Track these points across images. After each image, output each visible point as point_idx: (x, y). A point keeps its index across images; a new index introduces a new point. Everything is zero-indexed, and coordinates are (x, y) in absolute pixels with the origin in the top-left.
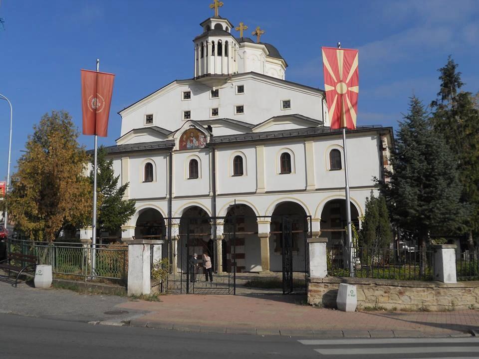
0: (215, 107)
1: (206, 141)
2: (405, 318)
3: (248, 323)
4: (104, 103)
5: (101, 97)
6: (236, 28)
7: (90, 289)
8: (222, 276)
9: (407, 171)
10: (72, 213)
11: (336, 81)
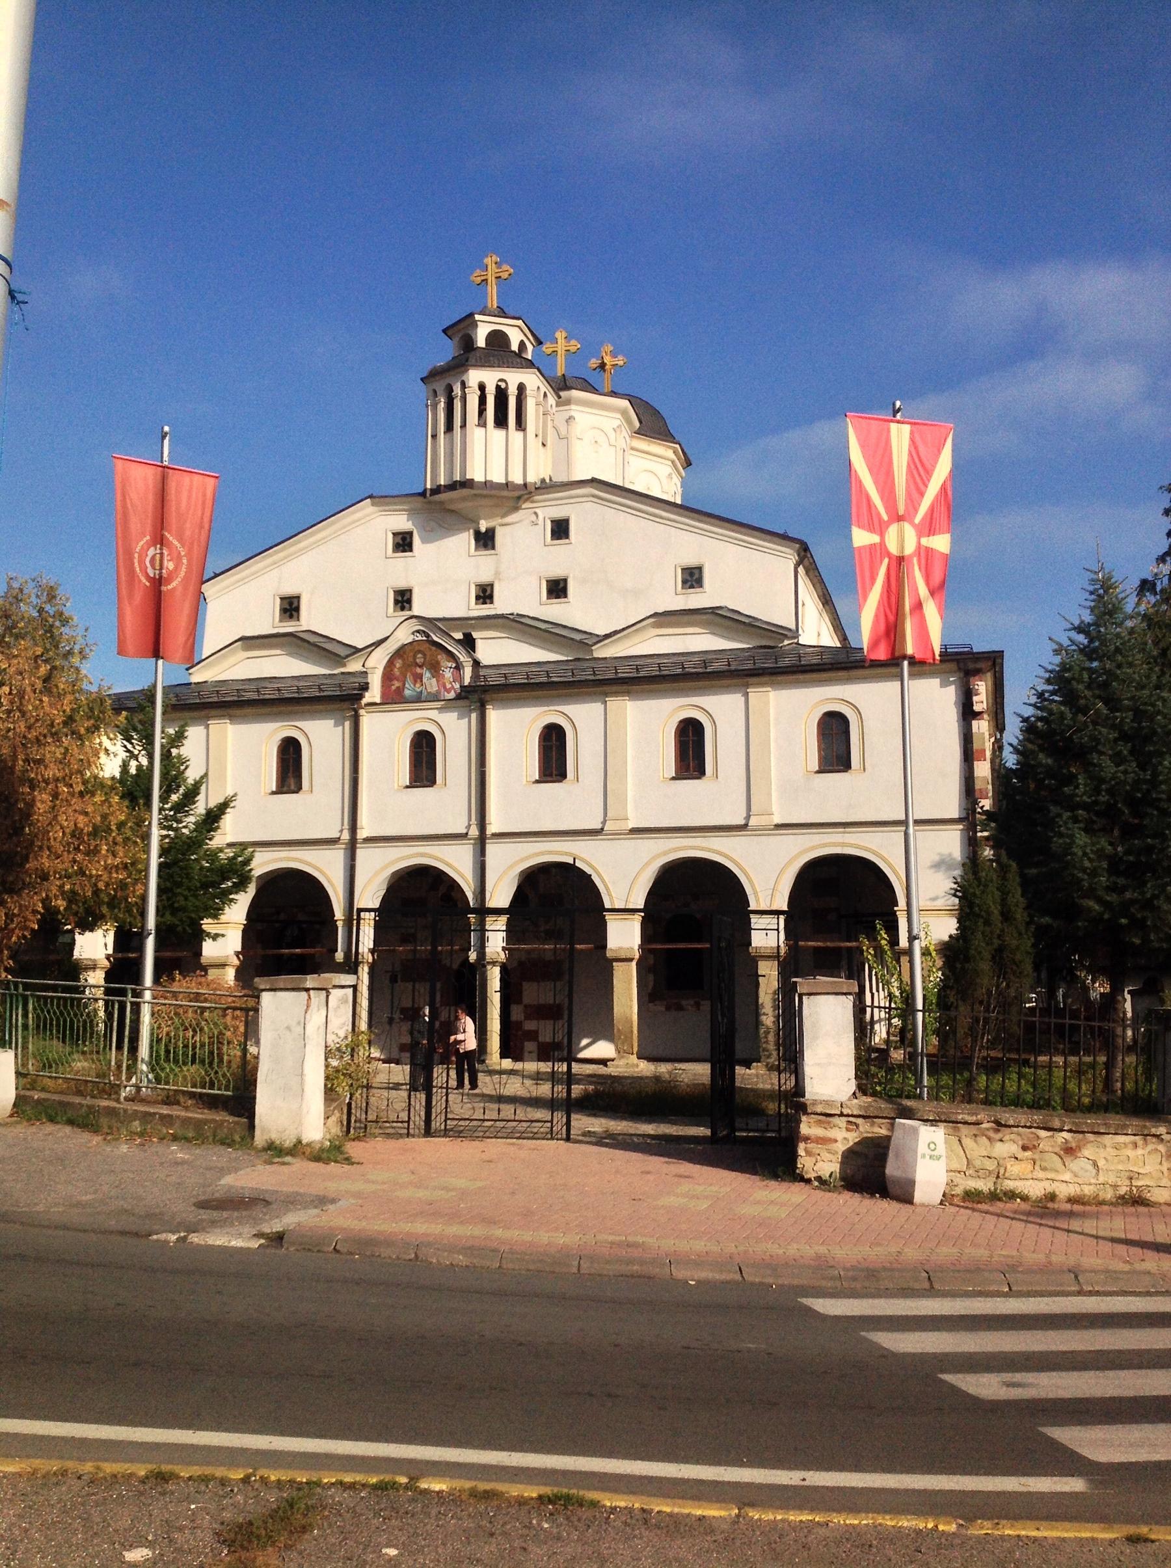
0: (485, 578)
1: (461, 679)
2: (1089, 1226)
3: (640, 1239)
4: (185, 561)
5: (176, 542)
6: (547, 348)
7: (136, 1125)
8: (515, 1077)
9: (1077, 787)
10: (67, 887)
11: (885, 517)
